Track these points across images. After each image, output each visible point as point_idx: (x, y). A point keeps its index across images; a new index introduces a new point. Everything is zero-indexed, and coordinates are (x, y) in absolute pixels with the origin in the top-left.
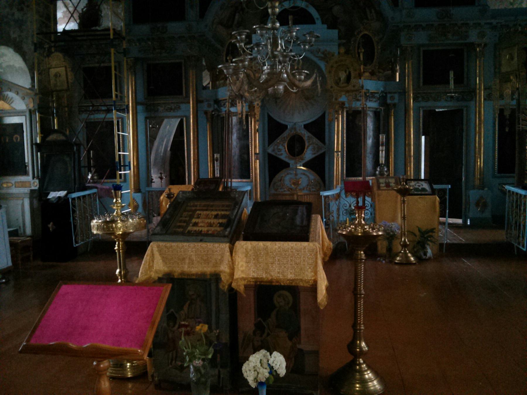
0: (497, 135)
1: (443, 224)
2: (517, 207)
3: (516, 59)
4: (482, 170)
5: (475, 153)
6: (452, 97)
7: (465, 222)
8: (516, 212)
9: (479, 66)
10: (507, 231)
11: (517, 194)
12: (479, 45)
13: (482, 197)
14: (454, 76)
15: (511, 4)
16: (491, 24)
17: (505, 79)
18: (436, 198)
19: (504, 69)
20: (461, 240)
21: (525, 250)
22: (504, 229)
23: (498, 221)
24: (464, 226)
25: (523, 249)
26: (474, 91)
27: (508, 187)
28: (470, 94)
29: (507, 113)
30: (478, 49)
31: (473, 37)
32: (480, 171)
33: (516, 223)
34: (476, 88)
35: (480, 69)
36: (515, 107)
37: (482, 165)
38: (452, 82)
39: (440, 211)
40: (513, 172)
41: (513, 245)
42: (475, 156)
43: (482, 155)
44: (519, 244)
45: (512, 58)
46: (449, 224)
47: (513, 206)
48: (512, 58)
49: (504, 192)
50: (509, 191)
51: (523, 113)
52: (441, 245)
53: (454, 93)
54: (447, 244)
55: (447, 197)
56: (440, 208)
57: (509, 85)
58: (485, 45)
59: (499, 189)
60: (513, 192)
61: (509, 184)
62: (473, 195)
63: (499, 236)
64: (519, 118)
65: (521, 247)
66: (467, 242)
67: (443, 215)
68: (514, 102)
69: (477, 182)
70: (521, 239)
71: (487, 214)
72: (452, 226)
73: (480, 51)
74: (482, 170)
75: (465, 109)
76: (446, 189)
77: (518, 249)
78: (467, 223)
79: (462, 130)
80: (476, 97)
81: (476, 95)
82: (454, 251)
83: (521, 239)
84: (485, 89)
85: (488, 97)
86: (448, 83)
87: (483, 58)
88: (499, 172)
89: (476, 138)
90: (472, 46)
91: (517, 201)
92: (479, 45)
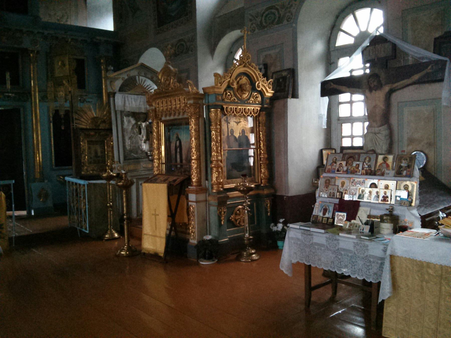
0: (52, 133)
1: (11, 217)
2: (77, 195)
3: (67, 66)
4: (41, 164)
5: (34, 148)
6: (9, 97)
7: (29, 213)
8: (76, 200)
9: (33, 71)
10: (70, 217)
11: (76, 184)
12: (32, 51)
13: (43, 189)
14: (10, 76)
15: (58, 20)
16: (43, 33)
17: (58, 83)
18: (1, 194)
19: (58, 73)
20: (28, 231)
21: (87, 232)
22: (67, 215)
23: (61, 208)
24: (29, 216)
25: (86, 231)
26: (30, 93)
27: (67, 179)
28: (26, 95)
29: (62, 113)
30: (31, 55)
31: (26, 43)
32: (40, 165)
33: (77, 209)
34: (31, 91)
35: (34, 73)
36: (69, 109)
37: (41, 160)
38: (8, 82)
39: (7, 206)
40: (71, 165)
41: (76, 229)
42: (34, 153)
43: (40, 151)
44: (82, 227)
45: (64, 65)
46: (16, 217)
47: (73, 194)
48: (64, 65)
49: (64, 183)
50: (69, 182)
51: (76, 113)
52: (10, 239)
53: (11, 93)
54: (15, 237)
55: (12, 192)
56: (7, 203)
57: (62, 88)
58: (38, 52)
59: (58, 181)
60: (73, 183)
61: (69, 175)
62: (35, 187)
63: (64, 221)
64: (73, 118)
65: (84, 230)
66: (35, 232)
67: (9, 208)
68: (67, 105)
69: (38, 176)
70: (83, 223)
71: (50, 203)
72: (19, 218)
73: (33, 56)
74: (41, 164)
75: (22, 109)
76: (10, 184)
77: (81, 231)
78: (31, 213)
79: (21, 128)
80: (31, 99)
81: (31, 96)
82: (25, 243)
83: (83, 223)
84: (39, 92)
85: (43, 99)
86: (5, 84)
87: (36, 64)
88: (56, 165)
89: (33, 136)
90: (25, 51)
91: (77, 190)
92: (32, 51)
